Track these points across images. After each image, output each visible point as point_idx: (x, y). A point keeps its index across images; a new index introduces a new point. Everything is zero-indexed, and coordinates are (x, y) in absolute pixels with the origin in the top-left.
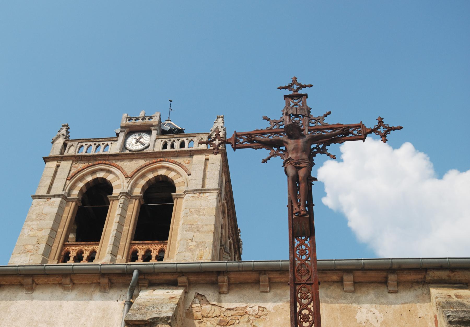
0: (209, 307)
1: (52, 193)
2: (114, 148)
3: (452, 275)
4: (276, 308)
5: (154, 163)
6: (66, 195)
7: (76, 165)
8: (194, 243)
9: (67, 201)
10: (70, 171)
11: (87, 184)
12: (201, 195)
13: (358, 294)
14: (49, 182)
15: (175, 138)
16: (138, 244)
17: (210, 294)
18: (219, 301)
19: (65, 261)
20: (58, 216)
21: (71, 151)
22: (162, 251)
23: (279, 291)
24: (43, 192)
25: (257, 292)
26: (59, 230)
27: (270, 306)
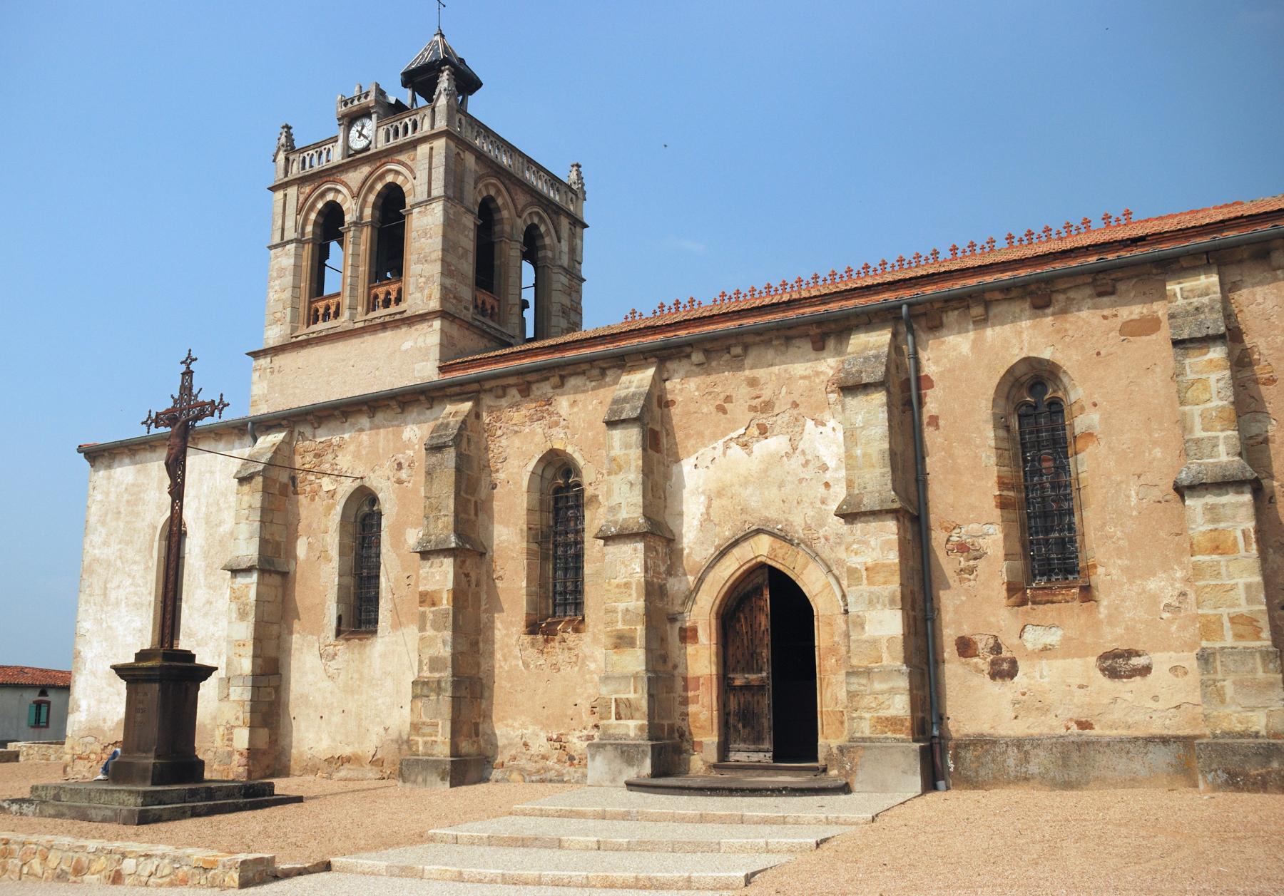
0: (308, 442)
1: (285, 239)
2: (336, 155)
3: (463, 388)
4: (350, 437)
5: (378, 167)
6: (300, 237)
7: (303, 190)
8: (423, 279)
9: (304, 244)
10: (298, 200)
11: (320, 213)
12: (428, 207)
13: (406, 414)
14: (280, 222)
15: (397, 121)
16: (378, 287)
17: (307, 430)
18: (314, 437)
19: (315, 322)
20: (297, 267)
21: (295, 171)
22: (400, 291)
23: (353, 420)
24: (277, 240)
25: (339, 423)
26: (302, 285)
27: (346, 436)
